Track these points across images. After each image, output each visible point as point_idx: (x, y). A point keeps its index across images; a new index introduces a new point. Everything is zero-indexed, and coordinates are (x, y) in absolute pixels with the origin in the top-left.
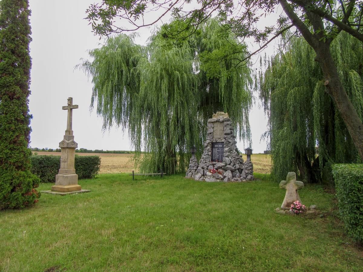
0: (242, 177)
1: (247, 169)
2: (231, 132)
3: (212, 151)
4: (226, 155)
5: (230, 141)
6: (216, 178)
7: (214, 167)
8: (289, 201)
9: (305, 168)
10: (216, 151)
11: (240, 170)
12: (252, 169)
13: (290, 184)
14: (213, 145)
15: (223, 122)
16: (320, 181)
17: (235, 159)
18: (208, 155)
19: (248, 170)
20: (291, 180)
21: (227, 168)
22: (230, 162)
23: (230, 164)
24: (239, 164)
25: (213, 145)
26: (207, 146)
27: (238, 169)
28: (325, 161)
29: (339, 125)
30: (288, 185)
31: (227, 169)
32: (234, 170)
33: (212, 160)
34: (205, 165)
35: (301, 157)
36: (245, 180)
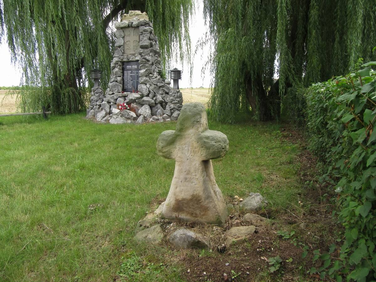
0: (165, 115)
1: (173, 102)
2: (151, 44)
3: (123, 75)
4: (142, 81)
5: (147, 57)
6: (126, 117)
7: (125, 99)
8: (181, 196)
9: (257, 98)
10: (128, 74)
11: (163, 104)
12: (181, 102)
13: (183, 142)
14: (123, 64)
15: (137, 27)
16: (277, 118)
17: (155, 87)
18: (116, 81)
19: (174, 103)
20: (187, 128)
21: (143, 101)
22: (147, 92)
23: (148, 96)
24: (162, 94)
25: (123, 64)
26: (114, 68)
27: (161, 103)
28: (288, 85)
29: (316, 17)
30: (178, 145)
31: (144, 103)
32: (154, 105)
33: (124, 90)
34: (111, 98)
35: (252, 80)
36: (169, 119)
